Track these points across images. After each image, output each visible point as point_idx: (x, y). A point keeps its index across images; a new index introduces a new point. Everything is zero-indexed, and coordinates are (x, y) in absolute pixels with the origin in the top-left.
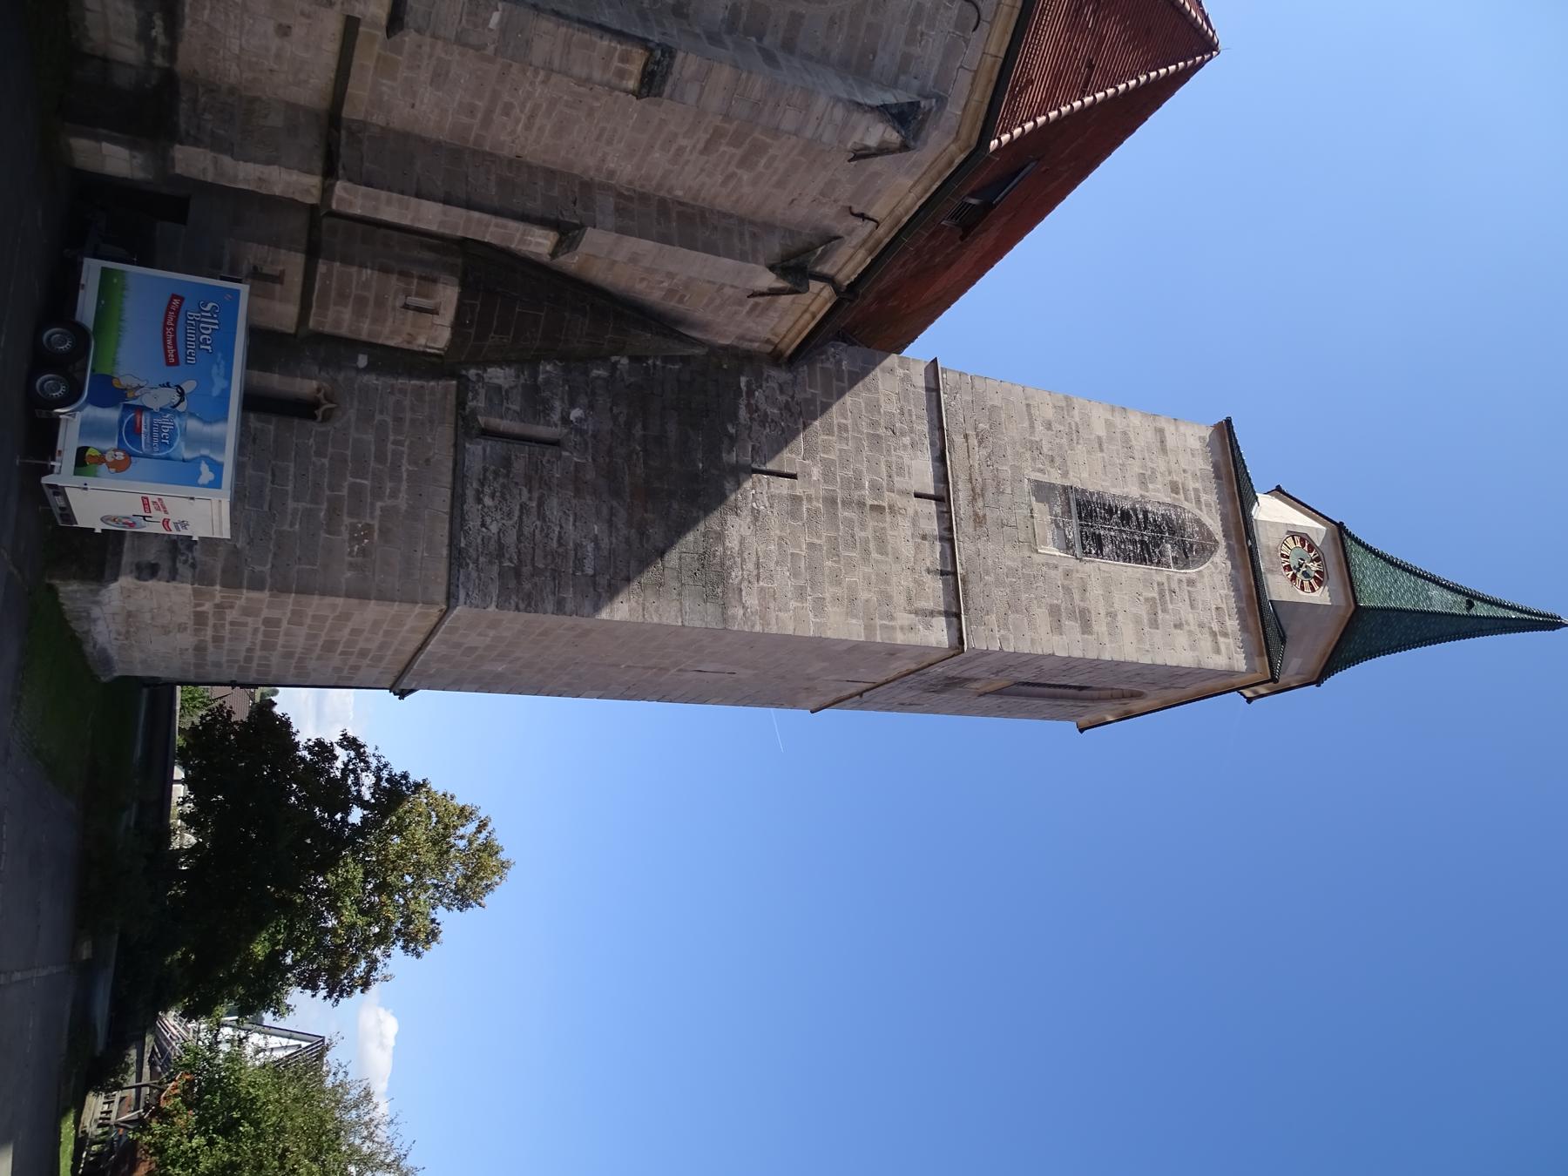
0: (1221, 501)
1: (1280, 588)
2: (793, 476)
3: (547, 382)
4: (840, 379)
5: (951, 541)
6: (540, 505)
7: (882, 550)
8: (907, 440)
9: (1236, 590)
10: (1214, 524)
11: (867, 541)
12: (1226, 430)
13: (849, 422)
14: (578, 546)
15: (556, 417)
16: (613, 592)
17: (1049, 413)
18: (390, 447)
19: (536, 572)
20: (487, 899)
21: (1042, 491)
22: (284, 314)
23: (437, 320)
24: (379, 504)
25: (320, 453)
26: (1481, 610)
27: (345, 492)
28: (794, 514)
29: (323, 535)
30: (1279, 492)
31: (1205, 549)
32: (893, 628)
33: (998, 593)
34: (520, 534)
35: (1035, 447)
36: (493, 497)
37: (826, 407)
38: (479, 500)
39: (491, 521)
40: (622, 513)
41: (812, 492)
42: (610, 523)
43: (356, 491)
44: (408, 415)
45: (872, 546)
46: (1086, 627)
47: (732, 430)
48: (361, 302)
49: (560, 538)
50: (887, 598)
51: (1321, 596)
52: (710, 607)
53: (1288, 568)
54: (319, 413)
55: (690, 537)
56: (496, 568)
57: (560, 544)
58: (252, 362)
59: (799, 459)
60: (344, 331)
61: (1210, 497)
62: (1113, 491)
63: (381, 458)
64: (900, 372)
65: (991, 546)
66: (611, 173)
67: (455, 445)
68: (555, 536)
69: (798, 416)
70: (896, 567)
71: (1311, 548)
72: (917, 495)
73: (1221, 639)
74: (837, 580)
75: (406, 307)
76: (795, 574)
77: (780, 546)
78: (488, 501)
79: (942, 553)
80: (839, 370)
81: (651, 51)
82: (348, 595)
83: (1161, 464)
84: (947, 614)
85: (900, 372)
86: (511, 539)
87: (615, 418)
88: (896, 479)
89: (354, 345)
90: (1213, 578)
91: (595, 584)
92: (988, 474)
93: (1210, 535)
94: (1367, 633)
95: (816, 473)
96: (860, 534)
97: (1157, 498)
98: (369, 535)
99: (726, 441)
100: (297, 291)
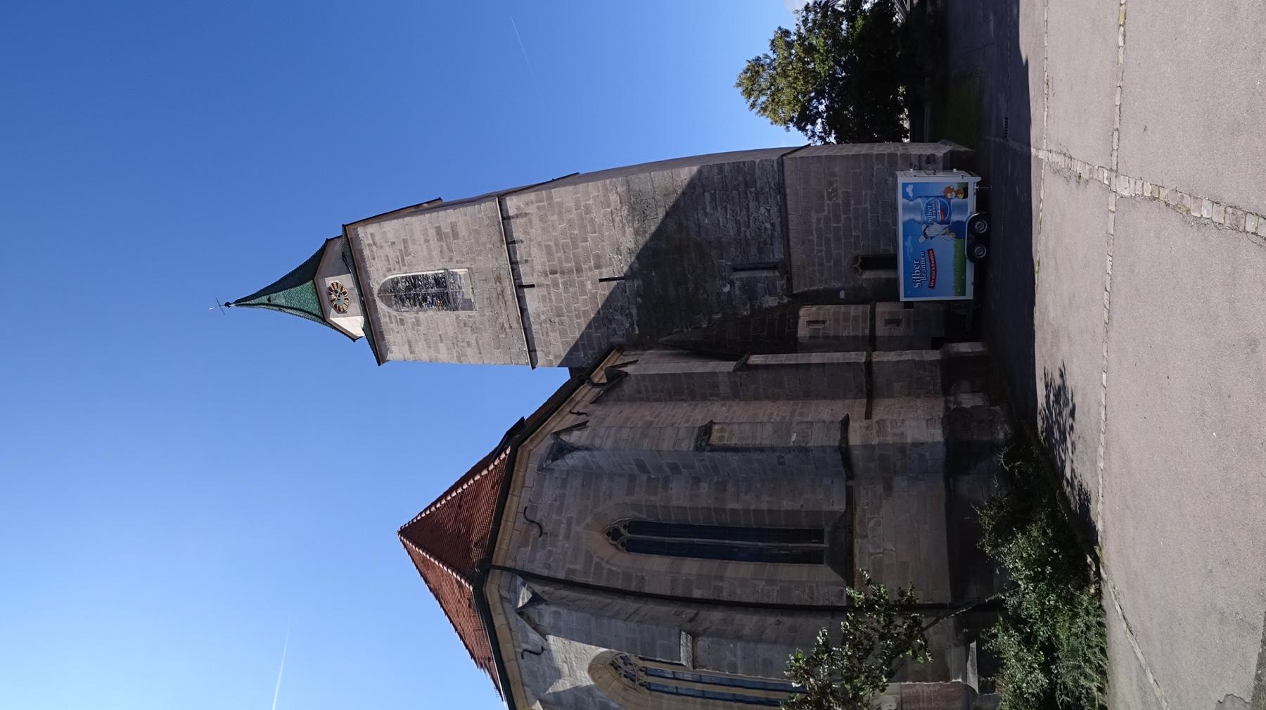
0: (378, 320)
1: (346, 281)
2: (601, 280)
3: (745, 305)
5: (512, 263)
6: (739, 229)
7: (548, 247)
8: (543, 317)
9: (366, 272)
10: (381, 306)
12: (380, 359)
13: (576, 321)
14: (715, 208)
15: (738, 284)
16: (692, 184)
17: (469, 351)
19: (736, 188)
20: (746, 65)
21: (468, 305)
22: (882, 308)
23: (807, 318)
25: (857, 237)
26: (264, 299)
28: (598, 257)
31: (383, 290)
33: (484, 238)
34: (748, 209)
35: (474, 330)
37: (589, 327)
38: (773, 225)
39: (764, 213)
42: (699, 226)
43: (837, 219)
46: (438, 230)
47: (639, 300)
48: (846, 319)
50: (543, 219)
51: (330, 281)
55: (653, 229)
56: (759, 185)
57: (726, 208)
58: (896, 280)
60: (853, 307)
61: (384, 320)
62: (430, 313)
64: (551, 357)
68: (729, 212)
69: (603, 318)
70: (539, 239)
72: (533, 286)
75: (824, 322)
76: (592, 220)
78: (768, 225)
79: (515, 254)
84: (509, 218)
85: (551, 357)
86: (752, 205)
89: (847, 302)
90: (379, 274)
91: (703, 186)
93: (381, 298)
94: (308, 272)
95: (589, 285)
100: (878, 318)
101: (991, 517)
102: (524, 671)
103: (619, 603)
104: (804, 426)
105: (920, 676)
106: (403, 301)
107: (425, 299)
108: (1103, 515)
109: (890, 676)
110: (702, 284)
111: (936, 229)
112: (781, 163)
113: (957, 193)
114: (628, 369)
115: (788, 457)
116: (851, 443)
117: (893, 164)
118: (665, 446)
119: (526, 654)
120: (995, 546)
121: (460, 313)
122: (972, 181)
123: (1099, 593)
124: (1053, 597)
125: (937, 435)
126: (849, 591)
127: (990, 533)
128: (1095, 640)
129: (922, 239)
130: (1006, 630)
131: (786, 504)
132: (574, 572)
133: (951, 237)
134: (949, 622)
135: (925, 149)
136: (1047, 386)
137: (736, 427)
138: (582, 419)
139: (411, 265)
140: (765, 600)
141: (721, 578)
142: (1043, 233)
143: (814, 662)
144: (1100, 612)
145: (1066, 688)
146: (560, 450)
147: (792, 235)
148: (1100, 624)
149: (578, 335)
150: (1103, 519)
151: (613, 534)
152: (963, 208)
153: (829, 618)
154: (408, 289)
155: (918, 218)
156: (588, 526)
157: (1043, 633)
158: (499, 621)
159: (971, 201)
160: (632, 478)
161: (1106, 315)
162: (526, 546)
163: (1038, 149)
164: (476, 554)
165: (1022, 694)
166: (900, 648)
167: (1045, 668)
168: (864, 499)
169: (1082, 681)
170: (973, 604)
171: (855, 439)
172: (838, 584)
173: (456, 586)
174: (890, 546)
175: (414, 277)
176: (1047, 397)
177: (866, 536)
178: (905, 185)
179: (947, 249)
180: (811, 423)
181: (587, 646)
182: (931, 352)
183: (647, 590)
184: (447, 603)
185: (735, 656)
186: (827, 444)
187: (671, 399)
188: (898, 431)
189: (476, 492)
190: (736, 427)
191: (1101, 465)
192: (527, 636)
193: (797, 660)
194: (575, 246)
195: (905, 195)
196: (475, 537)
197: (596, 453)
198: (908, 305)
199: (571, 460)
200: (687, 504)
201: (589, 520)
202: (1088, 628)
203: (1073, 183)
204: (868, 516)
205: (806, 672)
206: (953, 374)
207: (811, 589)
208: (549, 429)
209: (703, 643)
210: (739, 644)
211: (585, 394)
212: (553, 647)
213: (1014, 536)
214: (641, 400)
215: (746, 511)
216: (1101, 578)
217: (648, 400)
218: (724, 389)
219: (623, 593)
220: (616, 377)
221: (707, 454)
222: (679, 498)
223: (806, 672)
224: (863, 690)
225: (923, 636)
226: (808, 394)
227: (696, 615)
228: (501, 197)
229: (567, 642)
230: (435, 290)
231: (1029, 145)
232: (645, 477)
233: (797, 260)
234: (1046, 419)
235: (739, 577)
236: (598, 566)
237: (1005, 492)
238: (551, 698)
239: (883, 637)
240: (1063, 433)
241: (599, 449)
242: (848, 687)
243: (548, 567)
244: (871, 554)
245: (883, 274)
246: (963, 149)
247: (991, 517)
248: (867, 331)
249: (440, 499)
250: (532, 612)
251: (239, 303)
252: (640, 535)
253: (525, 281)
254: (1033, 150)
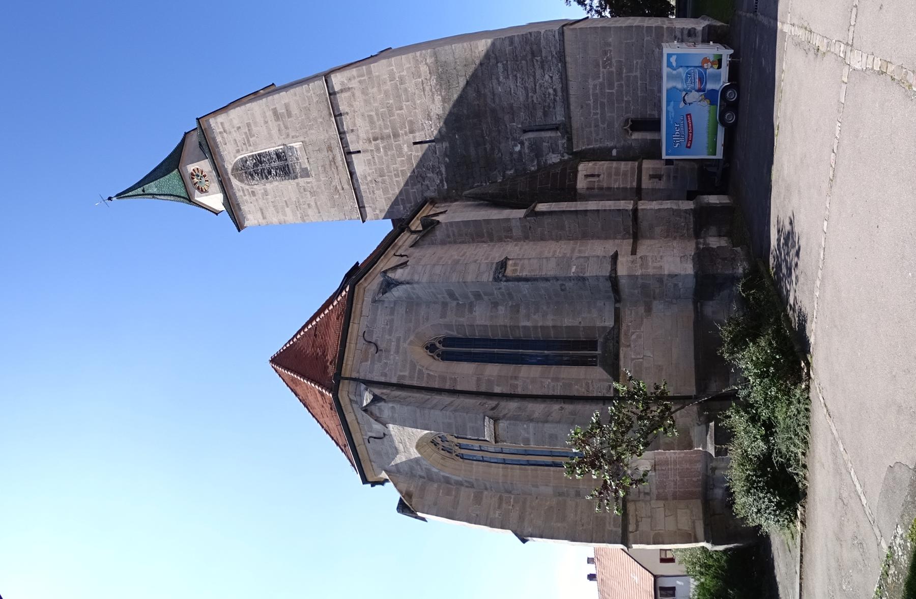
0: (234, 194)
1: (205, 165)
2: (415, 143)
3: (532, 161)
4: (402, 200)
5: (340, 133)
6: (527, 95)
7: (370, 117)
8: (369, 178)
9: (221, 156)
10: (235, 182)
11: (378, 120)
12: (239, 227)
13: (395, 179)
14: (507, 77)
15: (527, 144)
16: (487, 56)
18: (599, 111)
19: (524, 58)
21: (306, 173)
22: (648, 165)
23: (585, 173)
24: (601, 80)
25: (628, 102)
26: (139, 191)
27: (616, 84)
29: (623, 60)
30: (217, 213)
32: (358, 77)
33: (314, 114)
35: (313, 194)
36: (549, 94)
37: (406, 184)
38: (555, 90)
40: (489, 101)
41: (405, 138)
42: (494, 94)
43: (611, 86)
44: (593, 129)
45: (375, 118)
47: (447, 159)
48: (617, 174)
49: (516, 80)
50: (364, 92)
51: (191, 168)
52: (443, 59)
53: (205, 176)
54: (630, 123)
55: (455, 96)
56: (544, 55)
57: (516, 76)
58: (660, 141)
59: (414, 153)
60: (623, 163)
61: (239, 194)
62: (276, 183)
63: (603, 104)
64: (378, 212)
65: (322, 137)
66: (516, 245)
67: (570, 118)
68: (519, 80)
69: (417, 177)
71: (198, 188)
72: (359, 152)
73: (222, 130)
74: (386, 92)
75: (598, 176)
76: (406, 90)
77: (415, 104)
79: (343, 125)
80: (404, 204)
81: (503, 276)
82: (610, 28)
83: (261, 202)
86: (539, 72)
87: (500, 151)
88: (370, 157)
89: (618, 159)
90: (232, 155)
92: (330, 173)
94: (173, 162)
96: (381, 122)
97: (259, 186)
98: (604, 62)
99: (448, 153)
101: (730, 332)
102: (371, 452)
103: (437, 398)
104: (582, 260)
105: (669, 447)
106: (252, 175)
107: (270, 173)
108: (815, 333)
109: (646, 445)
110: (499, 144)
111: (694, 96)
112: (562, 33)
113: (713, 63)
114: (440, 218)
115: (569, 285)
116: (619, 273)
117: (659, 36)
118: (470, 278)
119: (371, 440)
120: (732, 353)
121: (300, 180)
122: (726, 53)
123: (808, 388)
124: (774, 389)
125: (688, 269)
126: (615, 385)
127: (729, 344)
128: (802, 421)
129: (682, 104)
130: (738, 412)
131: (568, 322)
132: (403, 377)
133: (706, 103)
134: (693, 408)
135: (687, 23)
136: (779, 231)
137: (526, 262)
138: (404, 259)
139: (255, 145)
140: (551, 393)
141: (516, 378)
142: (783, 101)
143: (589, 435)
144: (807, 401)
145: (780, 453)
146: (388, 285)
147: (572, 100)
148: (807, 410)
149: (397, 191)
150: (815, 335)
151: (431, 348)
152: (717, 78)
153: (601, 405)
154: (255, 165)
155: (679, 86)
156: (411, 343)
157: (765, 414)
158: (350, 418)
159: (725, 71)
160: (445, 305)
161: (831, 173)
162: (366, 360)
163: (783, 23)
164: (331, 370)
165: (747, 456)
166: (654, 426)
167: (765, 438)
168: (629, 316)
169: (792, 448)
170: (713, 394)
171: (622, 271)
172: (607, 381)
173: (319, 395)
174: (649, 354)
175: (260, 155)
176: (779, 240)
177: (629, 346)
178: (669, 56)
179: (703, 114)
180: (588, 258)
181: (414, 430)
182: (686, 202)
183: (459, 388)
184: (314, 408)
185: (528, 433)
186: (600, 274)
187: (473, 241)
188: (657, 265)
189: (326, 323)
190: (526, 262)
191: (817, 294)
192: (371, 427)
193: (576, 434)
194: (391, 114)
195: (669, 65)
196: (329, 357)
197: (415, 286)
198: (669, 162)
199: (397, 292)
200: (488, 323)
201: (412, 338)
202: (799, 413)
203: (811, 55)
204: (632, 330)
205: (583, 441)
206: (702, 220)
207: (587, 384)
208: (378, 269)
209: (502, 424)
210: (531, 425)
211: (406, 239)
212: (393, 433)
213: (747, 345)
214: (450, 243)
215: (535, 328)
216: (810, 378)
217: (455, 242)
218: (517, 232)
219: (439, 391)
220: (430, 225)
221: (503, 284)
222: (481, 319)
223: (583, 441)
224: (624, 454)
225: (672, 417)
226: (585, 236)
227: (497, 405)
228: (327, 76)
229: (401, 428)
230: (277, 164)
231: (776, 19)
232: (455, 303)
233: (576, 124)
234: (777, 258)
235: (530, 377)
236: (420, 372)
237: (741, 314)
238: (394, 468)
239: (640, 418)
240: (789, 269)
241: (418, 283)
242: (613, 452)
243: (386, 375)
244: (633, 360)
245: (649, 136)
246: (719, 24)
247: (730, 332)
248: (635, 184)
249: (299, 332)
250: (375, 409)
251: (119, 196)
252: (452, 348)
253: (352, 148)
254: (779, 24)
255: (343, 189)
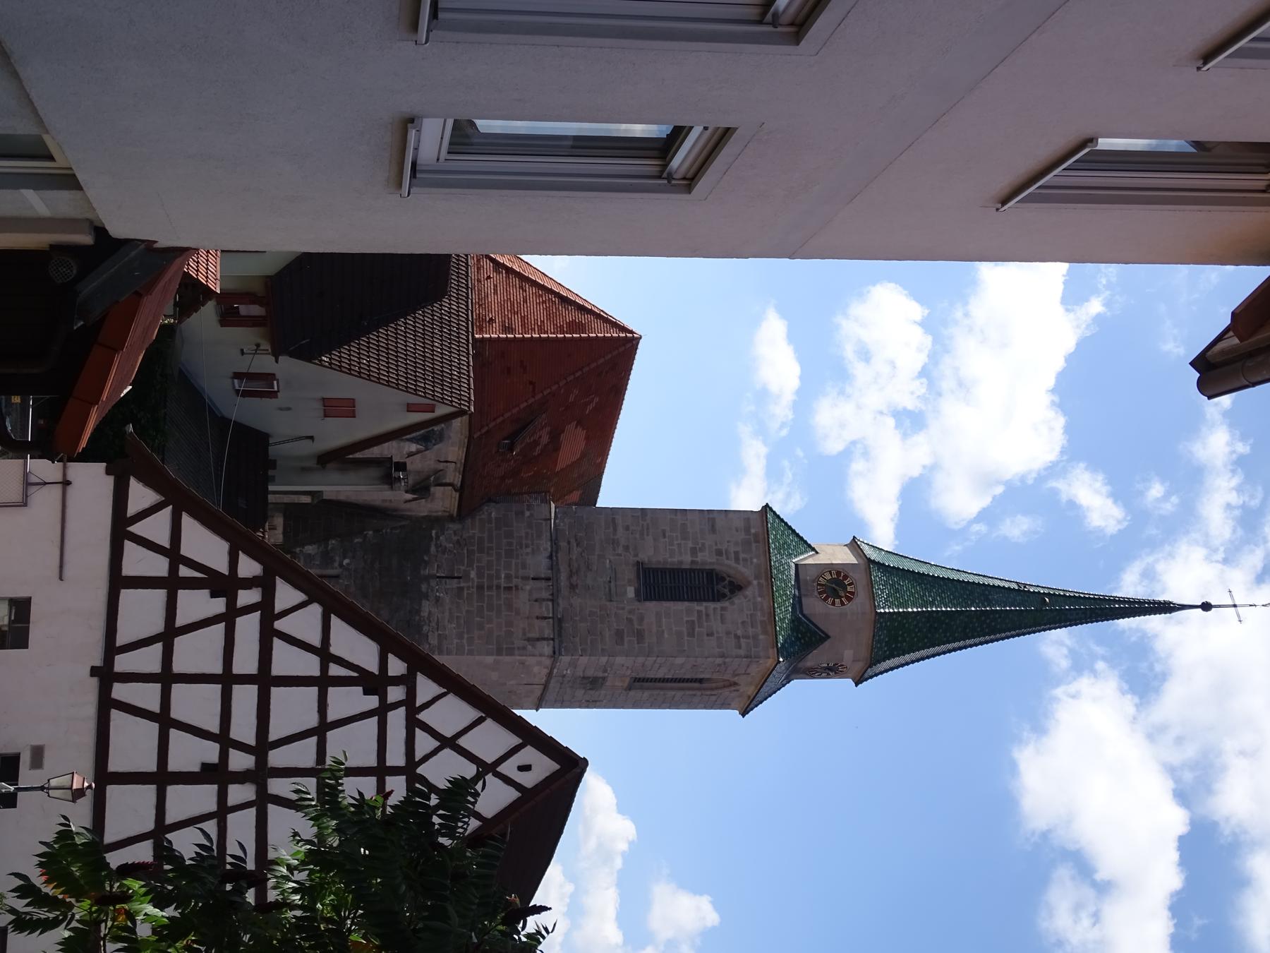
8: (529, 550)
15: (336, 564)
35: (615, 543)
47: (426, 558)
255: (569, 543)
